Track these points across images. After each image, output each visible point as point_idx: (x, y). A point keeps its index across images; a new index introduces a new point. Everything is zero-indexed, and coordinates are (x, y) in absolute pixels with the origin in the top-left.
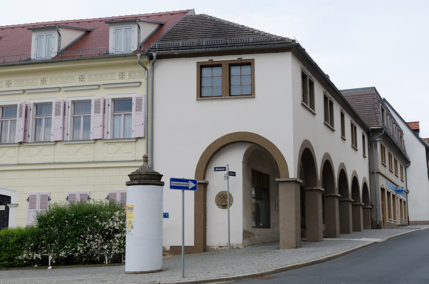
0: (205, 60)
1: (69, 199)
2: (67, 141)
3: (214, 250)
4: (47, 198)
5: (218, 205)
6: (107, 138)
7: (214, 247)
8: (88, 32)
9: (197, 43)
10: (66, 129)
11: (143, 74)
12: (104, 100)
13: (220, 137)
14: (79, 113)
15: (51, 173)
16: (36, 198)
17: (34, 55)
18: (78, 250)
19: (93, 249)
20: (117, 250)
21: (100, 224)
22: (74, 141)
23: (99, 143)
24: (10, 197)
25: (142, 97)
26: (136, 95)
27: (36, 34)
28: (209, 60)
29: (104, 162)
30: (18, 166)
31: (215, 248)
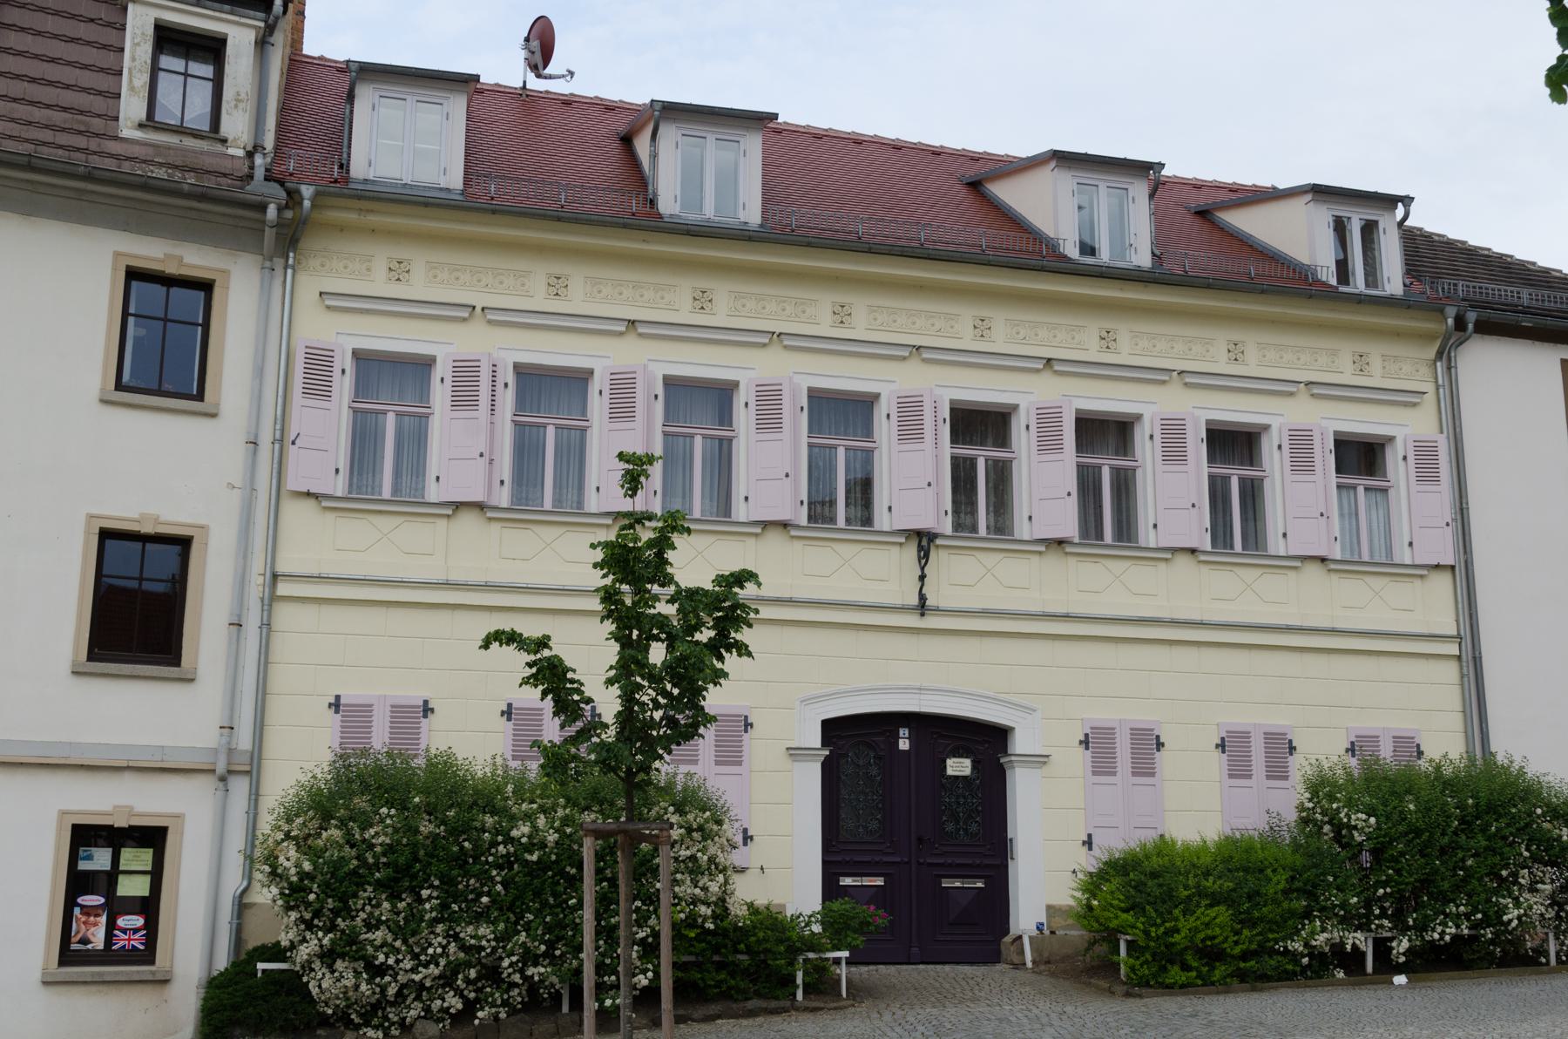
6: (1413, 561)
11: (1425, 371)
14: (539, 413)
16: (541, 720)
18: (1505, 918)
23: (468, 520)
25: (635, 372)
26: (751, 374)
29: (1067, 617)
30: (1066, 621)
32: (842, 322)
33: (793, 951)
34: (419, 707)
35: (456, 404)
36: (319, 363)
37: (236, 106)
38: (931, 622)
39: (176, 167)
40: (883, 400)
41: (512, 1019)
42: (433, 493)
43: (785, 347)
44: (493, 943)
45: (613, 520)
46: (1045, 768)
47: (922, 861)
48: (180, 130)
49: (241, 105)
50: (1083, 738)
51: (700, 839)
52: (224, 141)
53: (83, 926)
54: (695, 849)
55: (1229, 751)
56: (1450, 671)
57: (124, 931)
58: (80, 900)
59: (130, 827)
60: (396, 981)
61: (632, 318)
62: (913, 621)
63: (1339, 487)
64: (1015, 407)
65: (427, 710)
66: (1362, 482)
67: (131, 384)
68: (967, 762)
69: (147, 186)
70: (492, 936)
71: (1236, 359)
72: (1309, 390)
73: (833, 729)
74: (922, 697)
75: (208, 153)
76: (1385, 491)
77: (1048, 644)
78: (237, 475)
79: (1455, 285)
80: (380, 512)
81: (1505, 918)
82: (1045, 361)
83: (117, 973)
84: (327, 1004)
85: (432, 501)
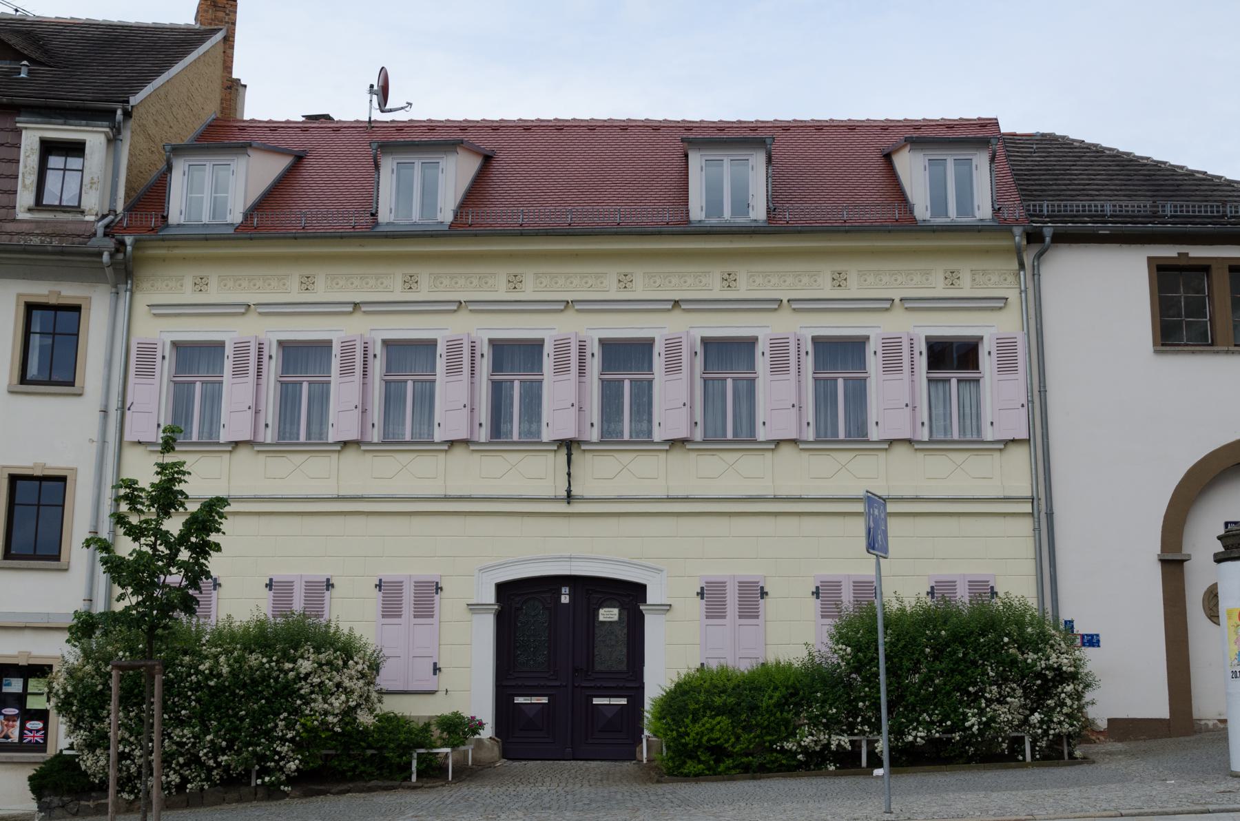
0: (1169, 252)
1: (822, 593)
3: (1208, 730)
4: (757, 590)
7: (1207, 722)
8: (299, 159)
9: (1152, 209)
10: (262, 414)
11: (1011, 279)
12: (259, 344)
13: (1219, 446)
15: (767, 525)
18: (967, 724)
19: (1000, 724)
20: (1066, 726)
21: (1020, 657)
22: (391, 442)
23: (243, 454)
26: (993, 330)
27: (922, 154)
28: (1178, 253)
29: (686, 499)
30: (684, 502)
31: (1210, 724)
32: (515, 288)
33: (406, 749)
34: (323, 582)
35: (1001, 370)
36: (148, 352)
37: (91, 187)
38: (576, 508)
39: (48, 235)
40: (985, 340)
41: (212, 789)
42: (989, 434)
44: (192, 740)
45: (558, 447)
46: (668, 614)
47: (576, 685)
48: (61, 208)
49: (94, 186)
50: (814, 590)
51: (329, 670)
54: (325, 677)
55: (707, 598)
56: (1026, 526)
57: (31, 731)
58: (3, 711)
59: (29, 665)
60: (134, 763)
61: (677, 299)
62: (563, 507)
63: (930, 380)
64: (981, 338)
65: (329, 585)
66: (954, 376)
67: (41, 379)
68: (616, 611)
69: (26, 250)
70: (191, 735)
71: (839, 286)
72: (903, 304)
73: (505, 590)
74: (573, 564)
75: (73, 222)
76: (977, 381)
77: (298, 519)
78: (95, 435)
79: (1041, 206)
80: (186, 452)
81: (967, 724)
82: (672, 303)
83: (21, 757)
84: (95, 777)
85: (989, 440)
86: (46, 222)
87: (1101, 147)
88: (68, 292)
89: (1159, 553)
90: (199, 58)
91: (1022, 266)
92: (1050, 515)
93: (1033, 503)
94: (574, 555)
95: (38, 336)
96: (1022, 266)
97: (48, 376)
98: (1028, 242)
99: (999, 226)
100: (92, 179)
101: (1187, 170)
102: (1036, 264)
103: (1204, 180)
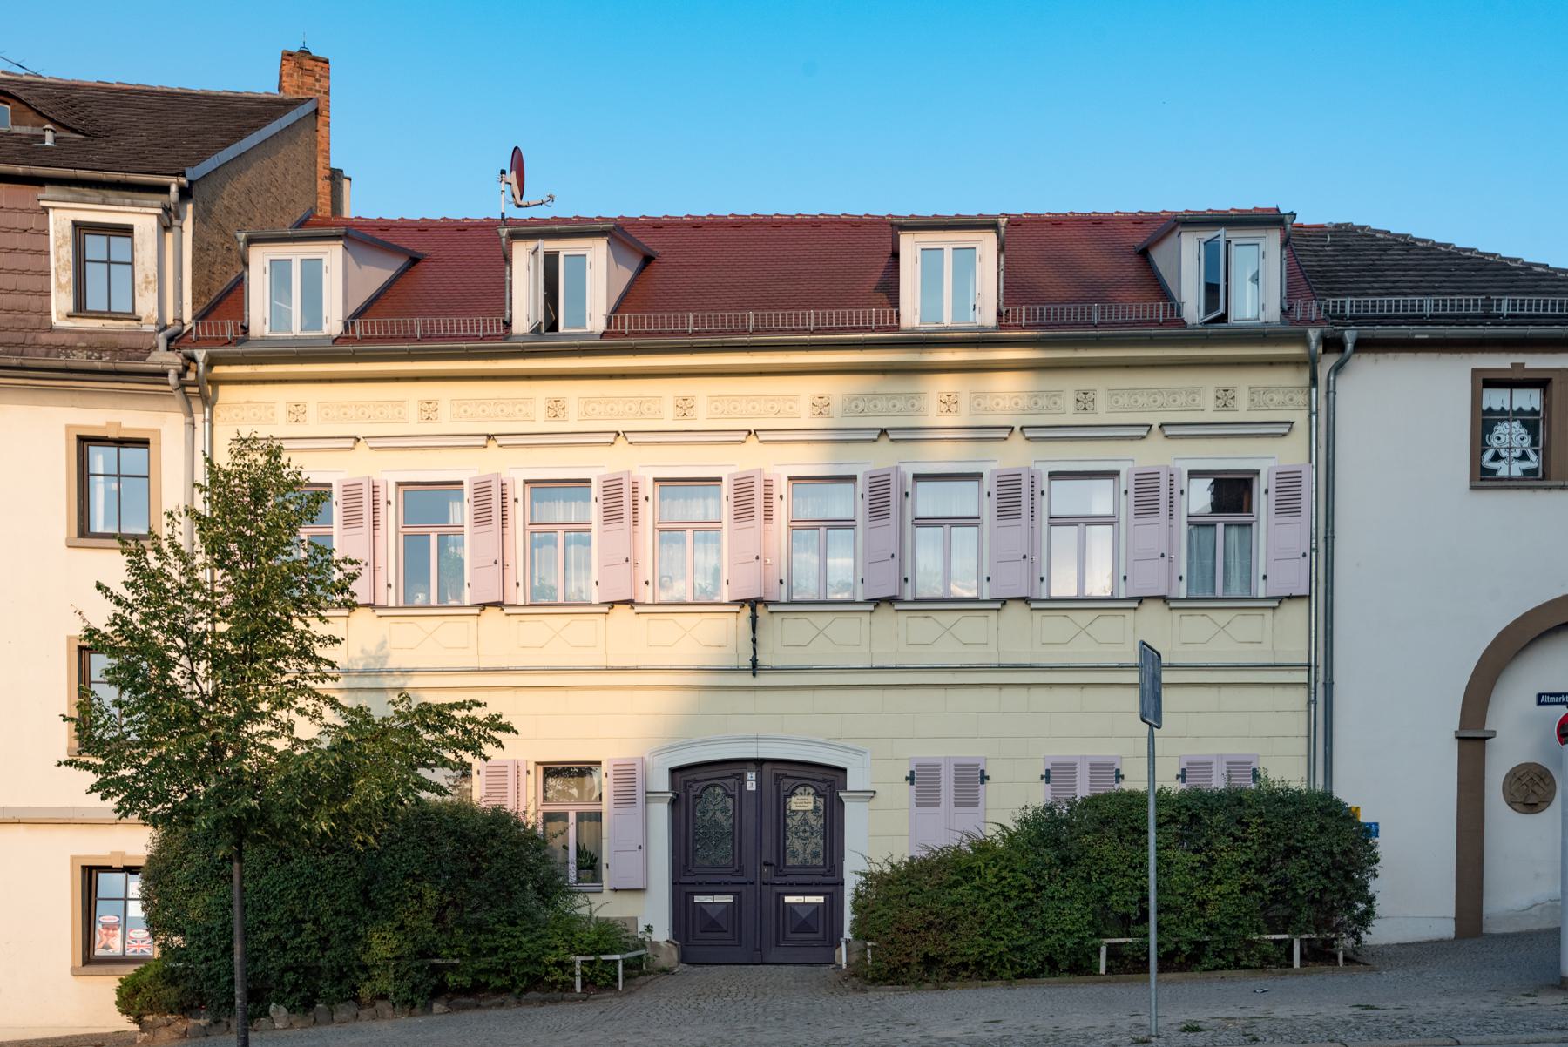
0: (1499, 362)
2: (386, 607)
5: (1511, 804)
17: (1267, 306)
23: (1014, 610)
24: (844, 770)
35: (1280, 512)
37: (146, 288)
38: (763, 679)
40: (1263, 475)
43: (892, 440)
52: (139, 320)
53: (105, 938)
56: (1299, 698)
61: (884, 427)
62: (747, 679)
71: (1085, 409)
74: (760, 745)
86: (92, 332)
87: (1412, 238)
88: (128, 418)
89: (1457, 729)
90: (282, 131)
91: (1314, 381)
92: (1329, 685)
93: (1309, 671)
94: (760, 735)
95: (101, 479)
96: (1314, 381)
97: (116, 527)
98: (1325, 351)
99: (1285, 331)
100: (147, 277)
101: (1523, 263)
102: (1332, 378)
103: (1545, 274)
